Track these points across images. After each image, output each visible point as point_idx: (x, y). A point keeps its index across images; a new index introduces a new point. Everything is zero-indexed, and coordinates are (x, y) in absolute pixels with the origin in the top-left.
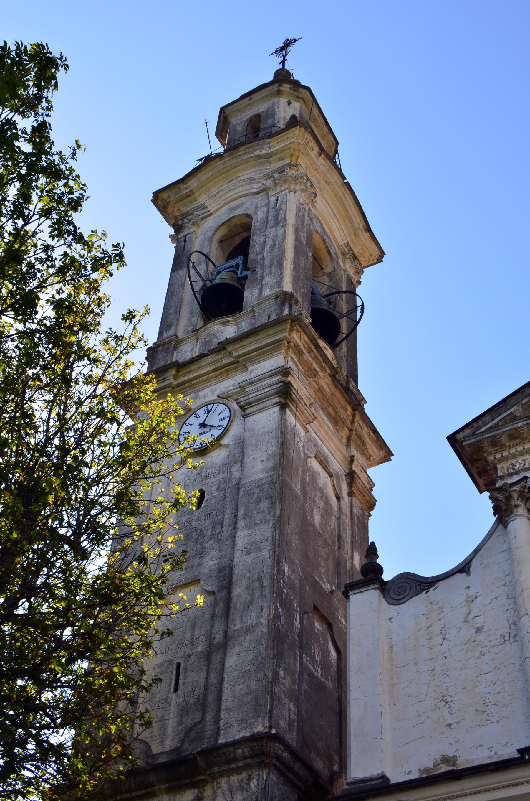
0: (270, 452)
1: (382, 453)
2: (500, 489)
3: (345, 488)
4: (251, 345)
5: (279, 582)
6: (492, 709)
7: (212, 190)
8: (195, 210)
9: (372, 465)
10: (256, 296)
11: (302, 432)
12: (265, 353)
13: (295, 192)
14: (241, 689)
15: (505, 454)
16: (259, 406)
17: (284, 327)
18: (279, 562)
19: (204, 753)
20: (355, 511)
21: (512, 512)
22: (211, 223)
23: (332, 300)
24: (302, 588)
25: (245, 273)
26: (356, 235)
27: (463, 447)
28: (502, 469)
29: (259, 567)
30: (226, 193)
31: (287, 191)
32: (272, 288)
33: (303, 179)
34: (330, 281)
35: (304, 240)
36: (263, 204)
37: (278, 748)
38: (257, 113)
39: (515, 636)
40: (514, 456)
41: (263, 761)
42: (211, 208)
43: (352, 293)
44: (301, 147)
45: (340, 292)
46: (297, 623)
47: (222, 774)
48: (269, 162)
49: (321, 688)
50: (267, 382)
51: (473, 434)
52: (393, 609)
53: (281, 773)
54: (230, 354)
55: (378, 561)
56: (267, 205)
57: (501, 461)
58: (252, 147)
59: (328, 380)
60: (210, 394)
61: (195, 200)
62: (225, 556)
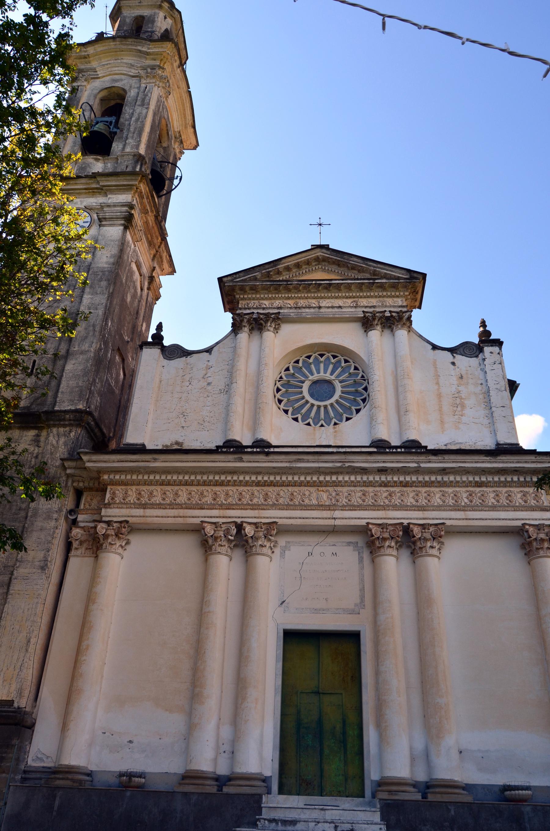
0: (113, 253)
1: (170, 270)
2: (239, 315)
3: (146, 284)
4: (112, 182)
5: (105, 330)
6: (206, 424)
7: (103, 60)
8: (88, 70)
9: (162, 275)
10: (120, 149)
11: (133, 246)
12: (120, 189)
13: (158, 87)
14: (73, 384)
15: (246, 296)
16: (111, 223)
17: (137, 178)
18: (107, 319)
19: (46, 412)
20: (149, 300)
21: (242, 329)
22: (97, 84)
23: (163, 166)
24: (115, 336)
25: (115, 130)
26: (186, 127)
27: (225, 286)
28: (242, 304)
29: (94, 319)
30: (112, 67)
31: (153, 84)
32: (132, 148)
33: (165, 80)
34: (164, 152)
35: (157, 122)
36: (136, 86)
37: (90, 419)
38: (142, 14)
39: (227, 391)
40: (250, 299)
41: (80, 424)
42: (100, 73)
43: (175, 165)
44: (169, 57)
45: (169, 163)
46: (109, 355)
47: (54, 426)
48: (146, 58)
49: (112, 392)
50: (118, 208)
51: (232, 281)
52: (166, 362)
53: (88, 432)
54: (98, 182)
55: (162, 333)
56: (139, 88)
57: (242, 299)
58: (137, 42)
59: (153, 218)
60: (79, 203)
61: (90, 63)
62: (74, 307)
